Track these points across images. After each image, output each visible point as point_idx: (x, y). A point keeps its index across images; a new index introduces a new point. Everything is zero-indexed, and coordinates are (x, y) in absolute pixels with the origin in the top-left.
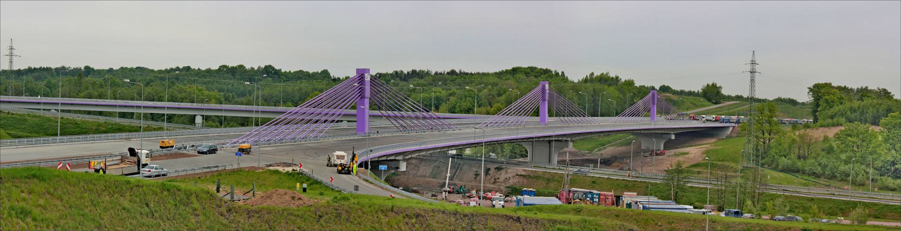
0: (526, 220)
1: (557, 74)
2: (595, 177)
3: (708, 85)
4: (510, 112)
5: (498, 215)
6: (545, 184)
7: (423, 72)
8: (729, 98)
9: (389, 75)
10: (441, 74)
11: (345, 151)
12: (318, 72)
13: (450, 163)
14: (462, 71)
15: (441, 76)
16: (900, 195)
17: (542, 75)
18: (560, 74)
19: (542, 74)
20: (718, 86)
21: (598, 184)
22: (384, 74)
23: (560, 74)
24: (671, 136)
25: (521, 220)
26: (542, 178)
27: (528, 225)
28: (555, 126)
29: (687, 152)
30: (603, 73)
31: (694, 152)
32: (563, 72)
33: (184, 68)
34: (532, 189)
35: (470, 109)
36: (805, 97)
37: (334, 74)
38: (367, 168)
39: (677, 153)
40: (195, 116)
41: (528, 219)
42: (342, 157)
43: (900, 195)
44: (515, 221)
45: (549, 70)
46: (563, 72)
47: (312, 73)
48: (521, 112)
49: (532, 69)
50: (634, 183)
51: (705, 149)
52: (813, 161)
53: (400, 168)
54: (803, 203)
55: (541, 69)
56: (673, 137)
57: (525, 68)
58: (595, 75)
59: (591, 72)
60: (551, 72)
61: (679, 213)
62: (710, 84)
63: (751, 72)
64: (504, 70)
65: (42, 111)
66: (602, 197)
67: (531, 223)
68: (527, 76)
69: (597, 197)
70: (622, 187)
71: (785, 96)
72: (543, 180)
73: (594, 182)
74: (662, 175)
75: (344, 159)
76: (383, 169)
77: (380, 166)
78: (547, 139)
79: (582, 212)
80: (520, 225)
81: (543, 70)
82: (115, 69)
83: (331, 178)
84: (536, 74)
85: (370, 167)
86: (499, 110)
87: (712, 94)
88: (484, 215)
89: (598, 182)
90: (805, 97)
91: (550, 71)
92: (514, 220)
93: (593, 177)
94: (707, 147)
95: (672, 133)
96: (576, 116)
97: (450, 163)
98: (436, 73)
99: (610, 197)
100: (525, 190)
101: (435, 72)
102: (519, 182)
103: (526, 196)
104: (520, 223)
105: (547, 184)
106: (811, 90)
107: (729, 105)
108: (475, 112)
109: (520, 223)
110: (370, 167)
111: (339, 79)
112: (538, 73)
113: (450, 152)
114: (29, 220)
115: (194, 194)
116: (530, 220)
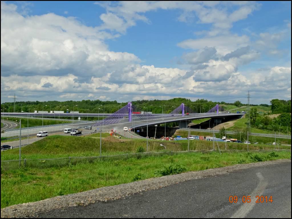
3: (236, 102)
8: (244, 105)
10: (152, 101)
16: (288, 137)
20: (240, 101)
28: (183, 117)
31: (231, 123)
32: (189, 99)
33: (70, 101)
36: (270, 104)
37: (118, 102)
40: (78, 117)
43: (288, 137)
52: (270, 125)
61: (205, 132)
62: (237, 101)
63: (248, 98)
65: (280, 136)
71: (264, 103)
73: (198, 133)
82: (46, 101)
87: (238, 104)
90: (270, 104)
91: (185, 99)
98: (150, 101)
106: (271, 102)
107: (243, 108)
111: (120, 103)
114: (59, 148)
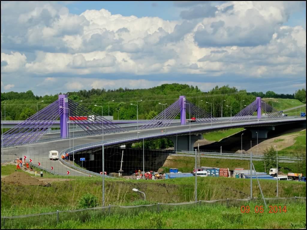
0: (169, 186)
1: (193, 88)
2: (218, 159)
3: (299, 91)
4: (168, 113)
5: (153, 183)
6: (185, 165)
7: (100, 90)
9: (76, 93)
11: (55, 150)
12: (24, 92)
13: (123, 154)
14: (127, 89)
15: (112, 93)
17: (182, 89)
18: (195, 88)
19: (182, 88)
21: (220, 163)
22: (73, 93)
23: (195, 88)
24: (272, 128)
25: (166, 186)
26: (183, 161)
27: (170, 188)
29: (283, 139)
30: (225, 86)
32: (197, 87)
34: (176, 168)
35: (134, 116)
38: (72, 160)
39: (277, 140)
41: (170, 185)
42: (55, 154)
44: (162, 186)
45: (187, 85)
46: (197, 87)
47: (20, 93)
48: (170, 116)
49: (175, 85)
50: (244, 161)
51: (296, 136)
53: (91, 158)
54: (32, 121)
55: (181, 85)
56: (274, 129)
57: (170, 85)
58: (219, 88)
59: (216, 86)
60: (189, 86)
64: (156, 87)
66: (220, 171)
67: (171, 187)
68: (172, 90)
69: (218, 171)
70: (237, 164)
72: (184, 162)
73: (218, 162)
74: (262, 155)
75: (57, 155)
76: (83, 160)
77: (81, 159)
78: (186, 134)
79: (204, 180)
80: (165, 188)
81: (183, 85)
83: (52, 167)
84: (179, 89)
85: (74, 159)
86: (154, 115)
88: (145, 184)
89: (220, 162)
92: (162, 186)
93: (217, 159)
94: (297, 135)
95: (273, 126)
96: (208, 118)
97: (123, 154)
99: (226, 172)
100: (171, 169)
101: (108, 90)
102: (168, 164)
103: (172, 173)
104: (165, 187)
105: (187, 164)
108: (137, 118)
109: (165, 187)
110: (74, 159)
112: (179, 88)
113: (122, 146)
115: (239, 103)
116: (171, 185)
